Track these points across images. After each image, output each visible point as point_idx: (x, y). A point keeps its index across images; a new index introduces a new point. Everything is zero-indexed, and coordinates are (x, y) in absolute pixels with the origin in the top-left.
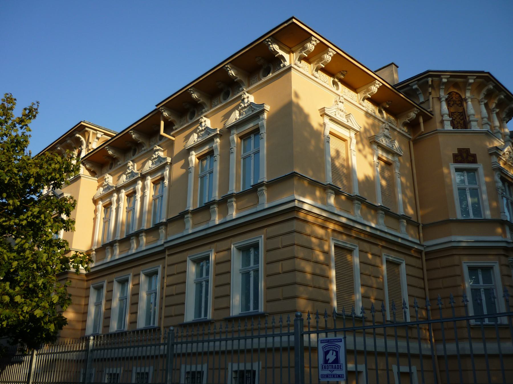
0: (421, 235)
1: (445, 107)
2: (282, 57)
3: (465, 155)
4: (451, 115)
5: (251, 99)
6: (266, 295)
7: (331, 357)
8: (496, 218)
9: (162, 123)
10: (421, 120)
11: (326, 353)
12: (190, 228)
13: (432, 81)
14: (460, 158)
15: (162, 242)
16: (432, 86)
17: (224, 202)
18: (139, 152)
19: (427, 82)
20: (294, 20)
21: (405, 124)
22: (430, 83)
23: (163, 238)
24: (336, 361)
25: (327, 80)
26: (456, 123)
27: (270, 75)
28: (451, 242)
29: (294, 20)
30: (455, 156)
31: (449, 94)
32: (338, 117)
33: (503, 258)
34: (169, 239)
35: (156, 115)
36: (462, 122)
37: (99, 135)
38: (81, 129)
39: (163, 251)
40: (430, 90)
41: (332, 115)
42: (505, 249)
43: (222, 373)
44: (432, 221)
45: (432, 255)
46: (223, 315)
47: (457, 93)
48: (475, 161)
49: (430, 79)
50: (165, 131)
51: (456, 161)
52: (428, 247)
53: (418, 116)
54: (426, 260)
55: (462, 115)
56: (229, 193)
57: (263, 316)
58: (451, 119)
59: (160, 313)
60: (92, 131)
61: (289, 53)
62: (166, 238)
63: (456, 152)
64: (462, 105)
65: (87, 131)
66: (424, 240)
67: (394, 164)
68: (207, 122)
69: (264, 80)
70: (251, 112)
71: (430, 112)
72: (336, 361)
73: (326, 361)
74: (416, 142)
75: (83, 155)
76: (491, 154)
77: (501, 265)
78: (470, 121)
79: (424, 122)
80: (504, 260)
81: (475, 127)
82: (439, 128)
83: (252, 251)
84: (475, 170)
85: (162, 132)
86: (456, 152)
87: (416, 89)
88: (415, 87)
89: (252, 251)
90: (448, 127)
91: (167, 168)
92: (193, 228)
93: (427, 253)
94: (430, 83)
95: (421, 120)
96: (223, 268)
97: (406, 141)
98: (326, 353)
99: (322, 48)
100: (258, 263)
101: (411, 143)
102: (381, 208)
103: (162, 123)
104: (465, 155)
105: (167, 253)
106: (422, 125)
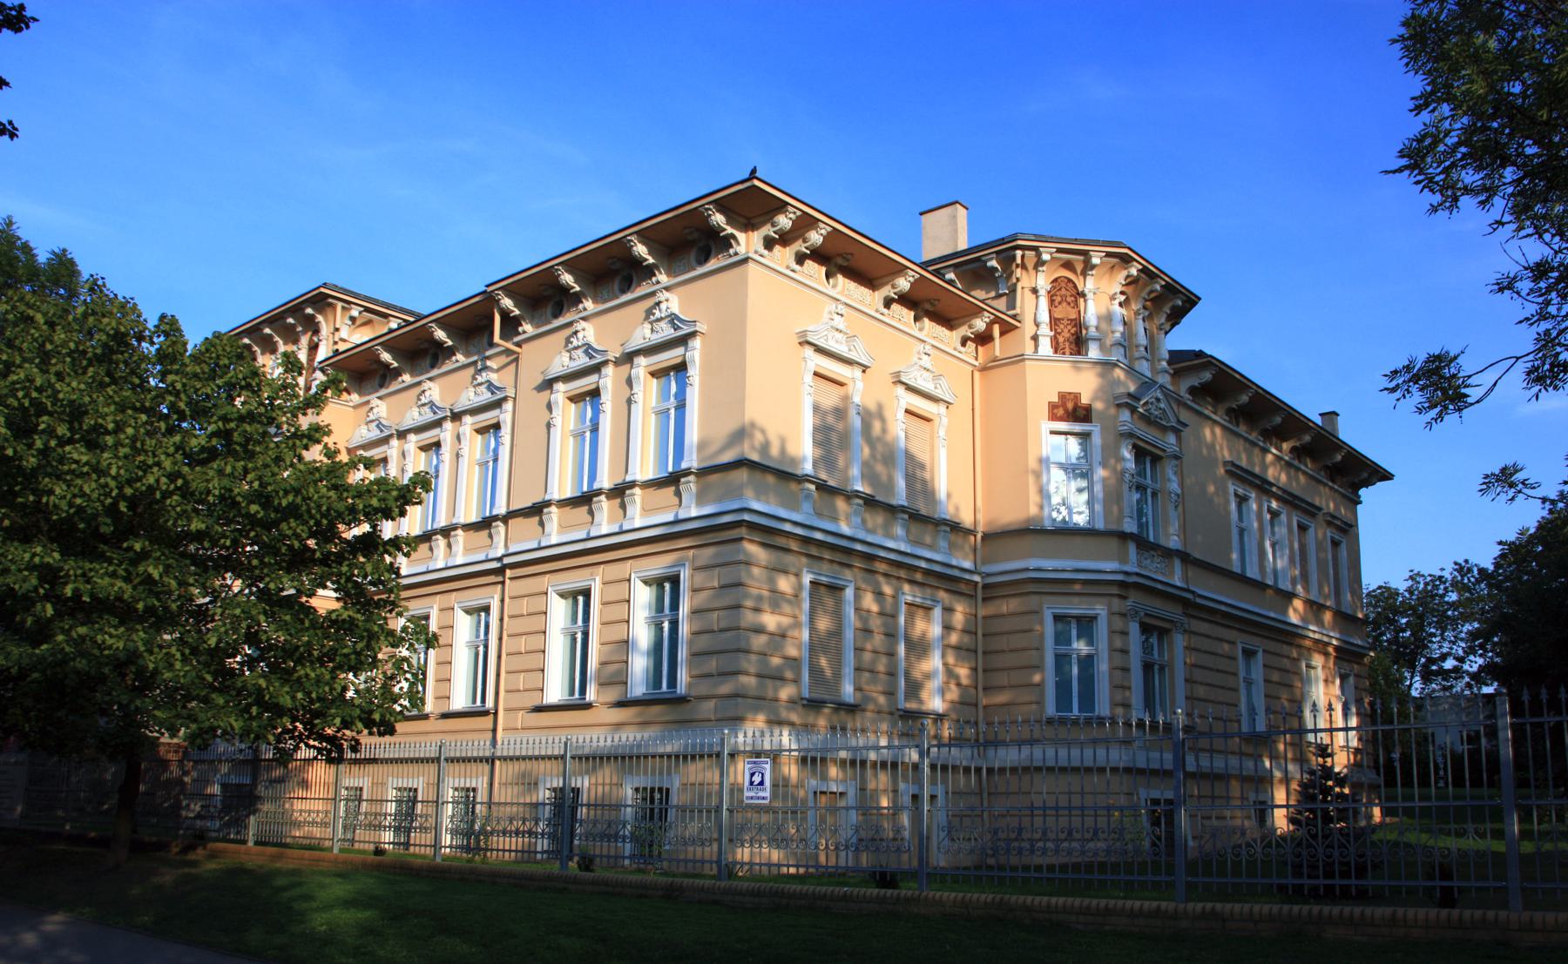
2: (733, 236)
4: (1054, 322)
5: (672, 303)
6: (690, 643)
7: (757, 779)
8: (1113, 527)
9: (497, 318)
11: (752, 775)
12: (557, 530)
15: (500, 552)
16: (1024, 267)
17: (619, 492)
19: (1014, 258)
20: (756, 183)
22: (1019, 261)
23: (499, 544)
24: (761, 783)
25: (814, 270)
27: (713, 264)
28: (1027, 570)
29: (756, 183)
30: (1053, 407)
31: (1055, 280)
32: (831, 345)
33: (1116, 601)
35: (488, 299)
37: (355, 313)
38: (320, 300)
40: (1018, 272)
41: (822, 343)
42: (1121, 584)
47: (1070, 280)
49: (1019, 253)
50: (502, 337)
51: (1053, 417)
52: (989, 575)
53: (990, 325)
56: (629, 478)
57: (683, 700)
60: (340, 305)
61: (741, 230)
62: (506, 545)
63: (1055, 399)
64: (1077, 305)
65: (331, 305)
66: (983, 563)
67: (936, 421)
68: (588, 332)
69: (701, 270)
71: (1014, 317)
72: (761, 783)
73: (752, 783)
75: (323, 353)
76: (1119, 406)
77: (1111, 614)
78: (1087, 340)
79: (1002, 334)
80: (1117, 604)
85: (497, 338)
86: (1055, 399)
90: (1045, 347)
91: (508, 406)
92: (560, 533)
93: (985, 587)
94: (1019, 261)
96: (618, 612)
98: (752, 775)
99: (805, 223)
100: (677, 609)
102: (902, 509)
103: (497, 318)
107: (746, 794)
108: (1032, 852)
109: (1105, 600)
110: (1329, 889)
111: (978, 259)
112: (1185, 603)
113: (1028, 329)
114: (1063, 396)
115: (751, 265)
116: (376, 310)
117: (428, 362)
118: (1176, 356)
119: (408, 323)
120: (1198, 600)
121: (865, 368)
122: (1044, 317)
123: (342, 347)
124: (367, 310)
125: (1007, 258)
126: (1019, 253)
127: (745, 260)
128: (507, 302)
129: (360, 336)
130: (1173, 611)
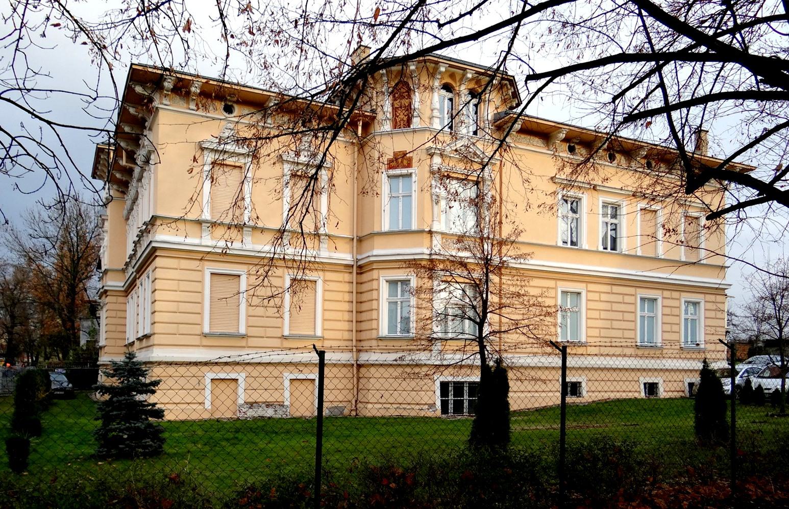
4: (395, 109)
26: (398, 119)
36: (405, 119)
54: (357, 274)
55: (407, 110)
90: (388, 127)
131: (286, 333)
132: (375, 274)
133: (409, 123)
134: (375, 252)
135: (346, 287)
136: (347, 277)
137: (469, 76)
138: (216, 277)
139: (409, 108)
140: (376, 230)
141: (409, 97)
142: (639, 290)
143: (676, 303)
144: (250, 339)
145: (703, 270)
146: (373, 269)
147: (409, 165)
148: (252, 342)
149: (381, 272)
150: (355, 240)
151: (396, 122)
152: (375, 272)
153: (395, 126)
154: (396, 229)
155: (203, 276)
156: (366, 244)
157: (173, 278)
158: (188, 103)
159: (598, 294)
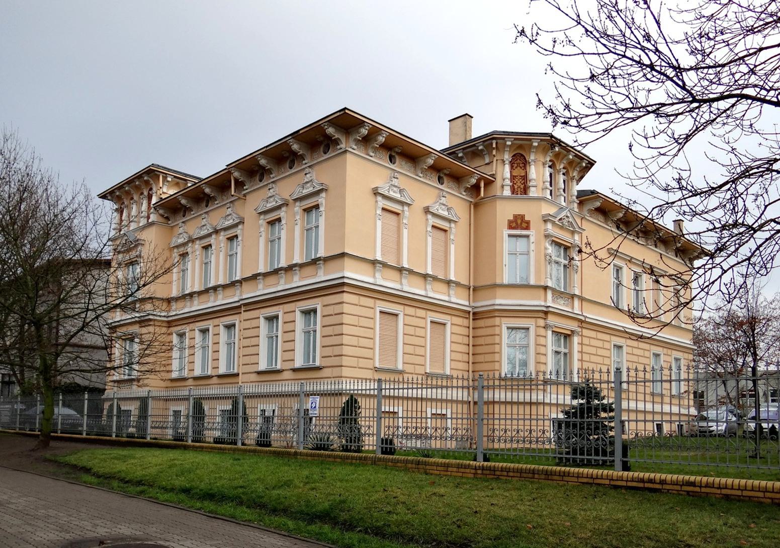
0: (471, 296)
1: (507, 168)
3: (519, 221)
4: (513, 178)
10: (482, 185)
13: (497, 143)
14: (514, 225)
18: (213, 205)
21: (467, 190)
22: (494, 146)
24: (315, 407)
26: (516, 187)
30: (510, 222)
34: (244, 297)
36: (522, 186)
39: (239, 307)
40: (494, 152)
41: (386, 193)
43: (322, 406)
44: (489, 283)
45: (477, 316)
46: (289, 365)
48: (528, 228)
51: (510, 227)
52: (476, 307)
54: (473, 319)
55: (524, 179)
57: (319, 369)
58: (511, 184)
59: (239, 361)
70: (312, 188)
72: (315, 407)
74: (476, 205)
81: (533, 192)
82: (499, 193)
83: (312, 314)
84: (527, 236)
87: (482, 150)
88: (480, 148)
89: (312, 314)
90: (507, 192)
93: (474, 314)
94: (494, 146)
95: (482, 185)
97: (468, 204)
101: (472, 206)
104: (519, 221)
105: (243, 309)
106: (482, 189)
107: (310, 412)
108: (537, 442)
109: (534, 320)
110: (604, 462)
111: (474, 145)
112: (581, 321)
113: (499, 182)
114: (515, 217)
115: (348, 155)
116: (180, 178)
117: (258, 178)
118: (581, 194)
119: (196, 183)
120: (587, 320)
121: (409, 205)
122: (508, 175)
123: (164, 196)
124: (175, 177)
125: (489, 148)
126: (494, 142)
127: (346, 151)
128: (236, 174)
129: (172, 192)
130: (573, 326)
131: (377, 365)
132: (497, 321)
133: (525, 190)
134: (498, 301)
135: (465, 331)
136: (465, 322)
137: (509, 143)
138: (435, 325)
139: (525, 178)
140: (498, 282)
141: (525, 167)
142: (429, 313)
143: (369, 313)
144: (325, 370)
145: (682, 332)
146: (343, 292)
147: (527, 228)
148: (326, 373)
149: (503, 319)
150: (471, 289)
151: (514, 189)
152: (497, 319)
153: (513, 191)
154: (514, 282)
155: (375, 313)
156: (480, 294)
157: (355, 313)
158: (366, 149)
159: (592, 344)
